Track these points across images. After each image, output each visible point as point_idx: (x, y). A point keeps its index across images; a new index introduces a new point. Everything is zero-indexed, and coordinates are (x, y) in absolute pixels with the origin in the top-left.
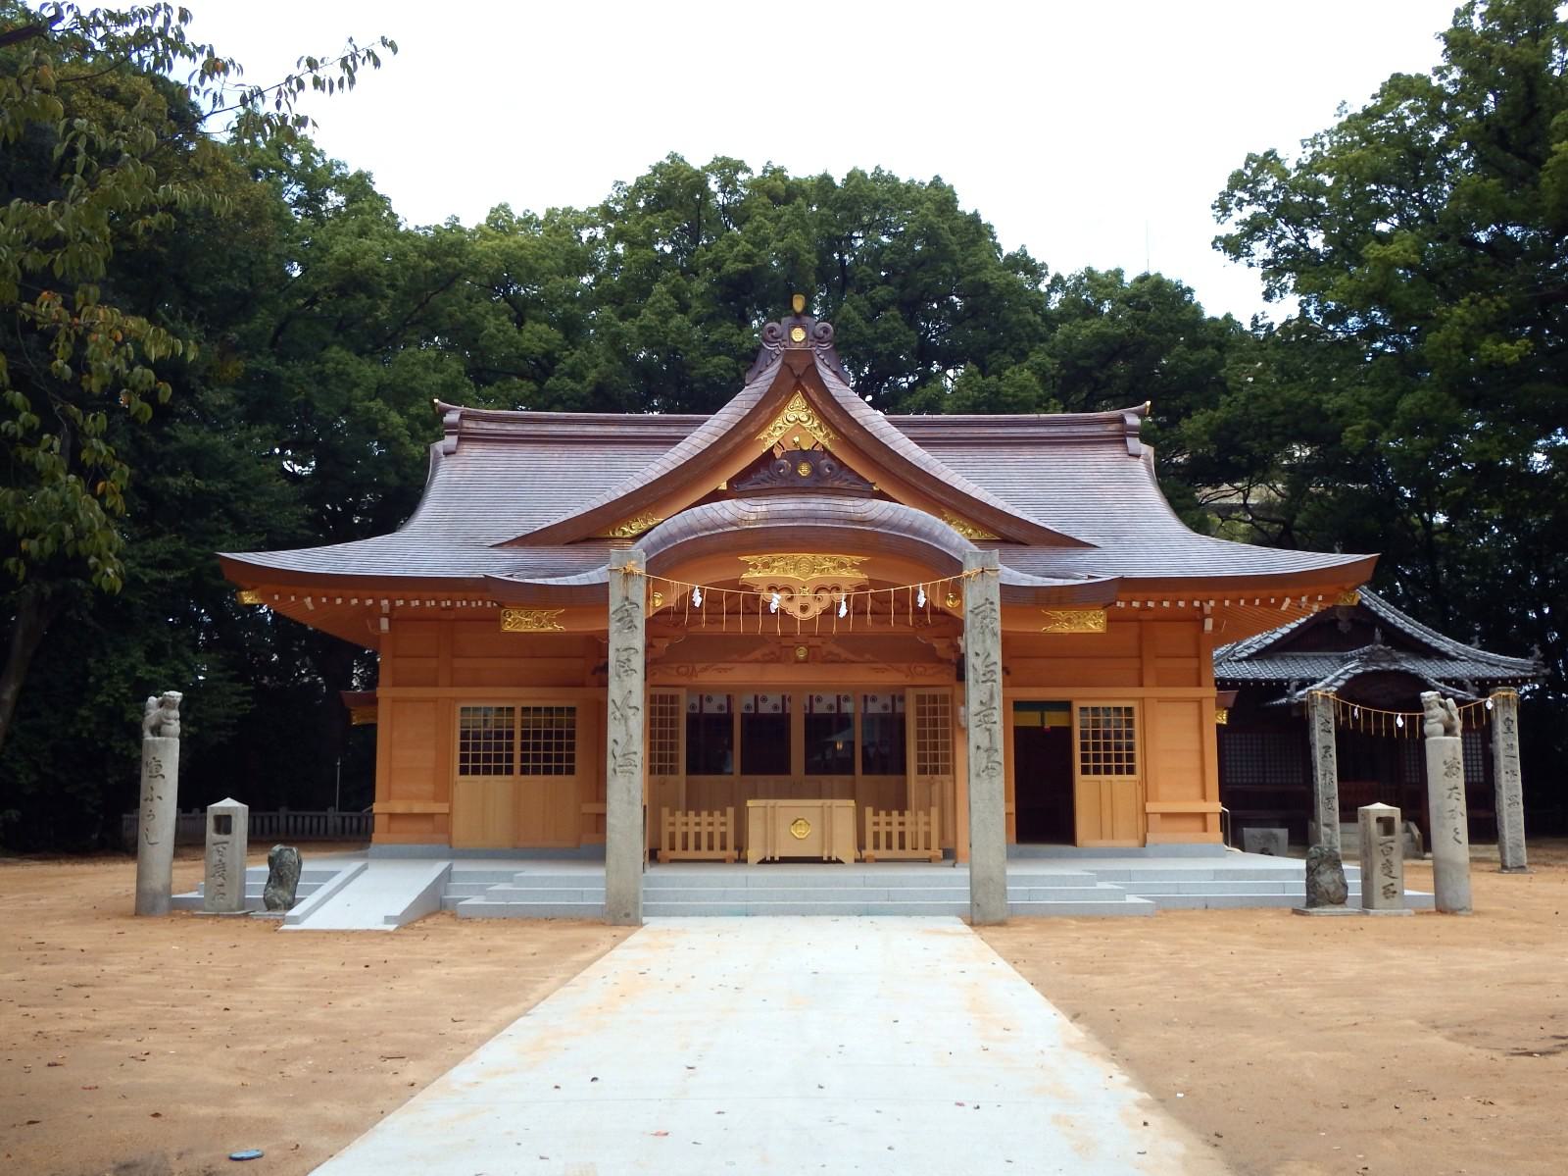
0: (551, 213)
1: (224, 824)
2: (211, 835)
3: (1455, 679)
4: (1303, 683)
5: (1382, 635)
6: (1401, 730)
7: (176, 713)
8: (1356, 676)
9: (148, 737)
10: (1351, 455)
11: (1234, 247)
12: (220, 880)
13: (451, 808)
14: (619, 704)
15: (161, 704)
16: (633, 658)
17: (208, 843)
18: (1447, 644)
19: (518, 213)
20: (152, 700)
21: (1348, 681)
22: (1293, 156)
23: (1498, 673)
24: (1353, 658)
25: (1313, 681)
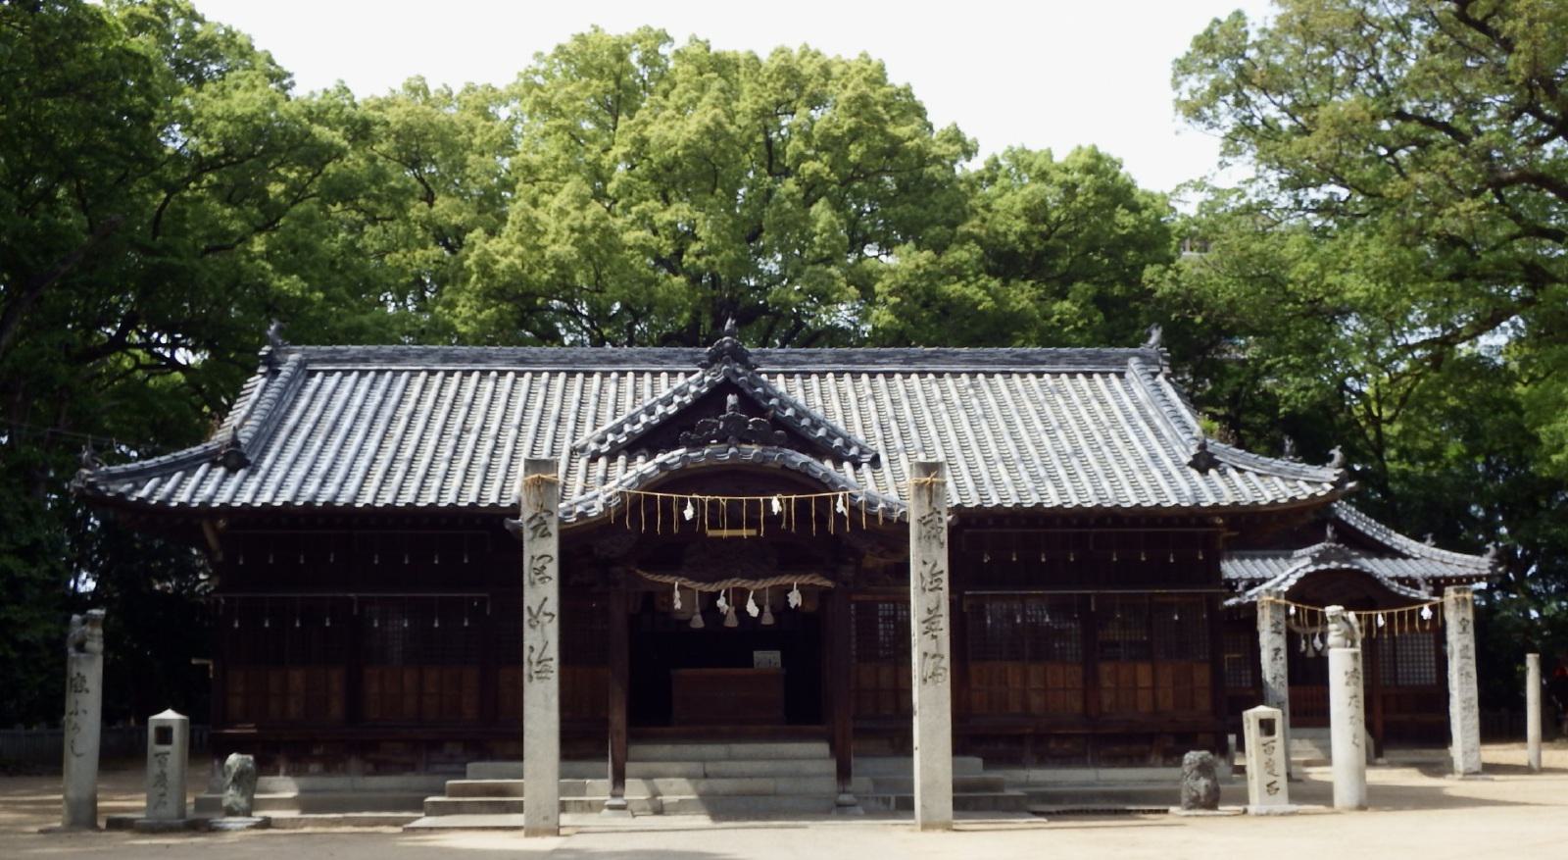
0: (470, 89)
1: (164, 734)
2: (154, 748)
3: (1409, 578)
4: (1252, 583)
5: (1334, 532)
6: (1380, 630)
7: (99, 631)
8: (1308, 575)
9: (71, 650)
10: (211, 416)
11: (1194, 111)
12: (162, 790)
13: (1362, 777)
14: (535, 610)
15: (84, 622)
16: (548, 566)
17: (150, 755)
18: (1399, 540)
19: (434, 86)
20: (76, 617)
21: (1300, 580)
22: (1224, 18)
23: (1450, 572)
24: (1304, 556)
25: (1263, 580)
